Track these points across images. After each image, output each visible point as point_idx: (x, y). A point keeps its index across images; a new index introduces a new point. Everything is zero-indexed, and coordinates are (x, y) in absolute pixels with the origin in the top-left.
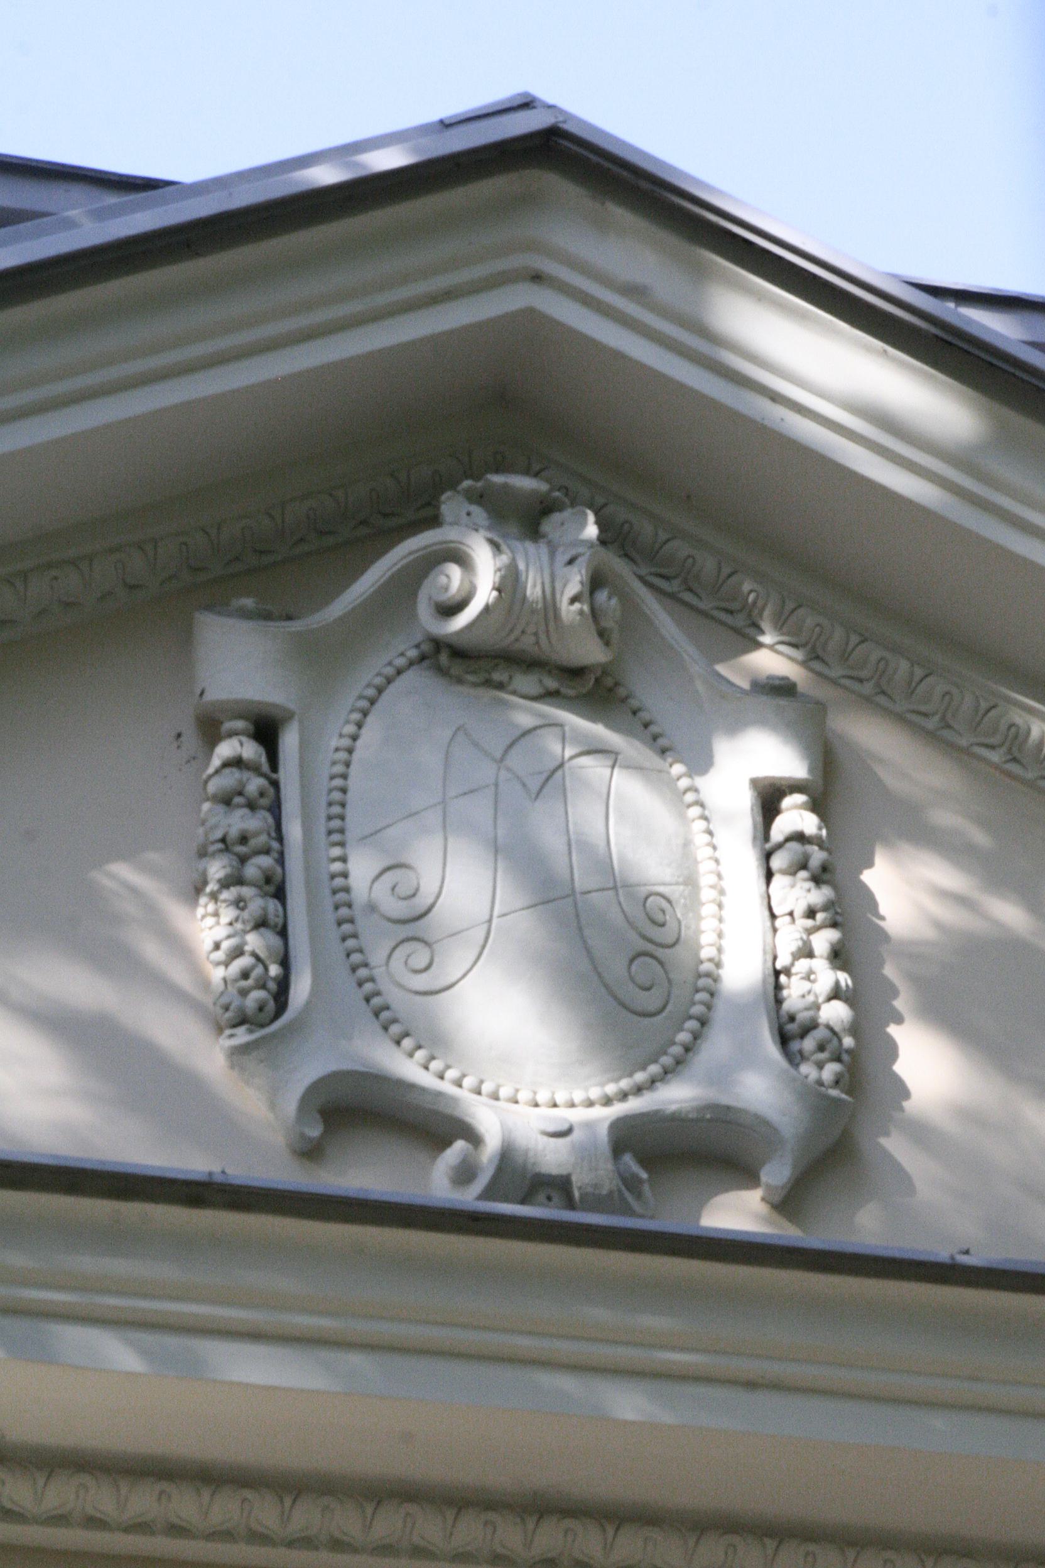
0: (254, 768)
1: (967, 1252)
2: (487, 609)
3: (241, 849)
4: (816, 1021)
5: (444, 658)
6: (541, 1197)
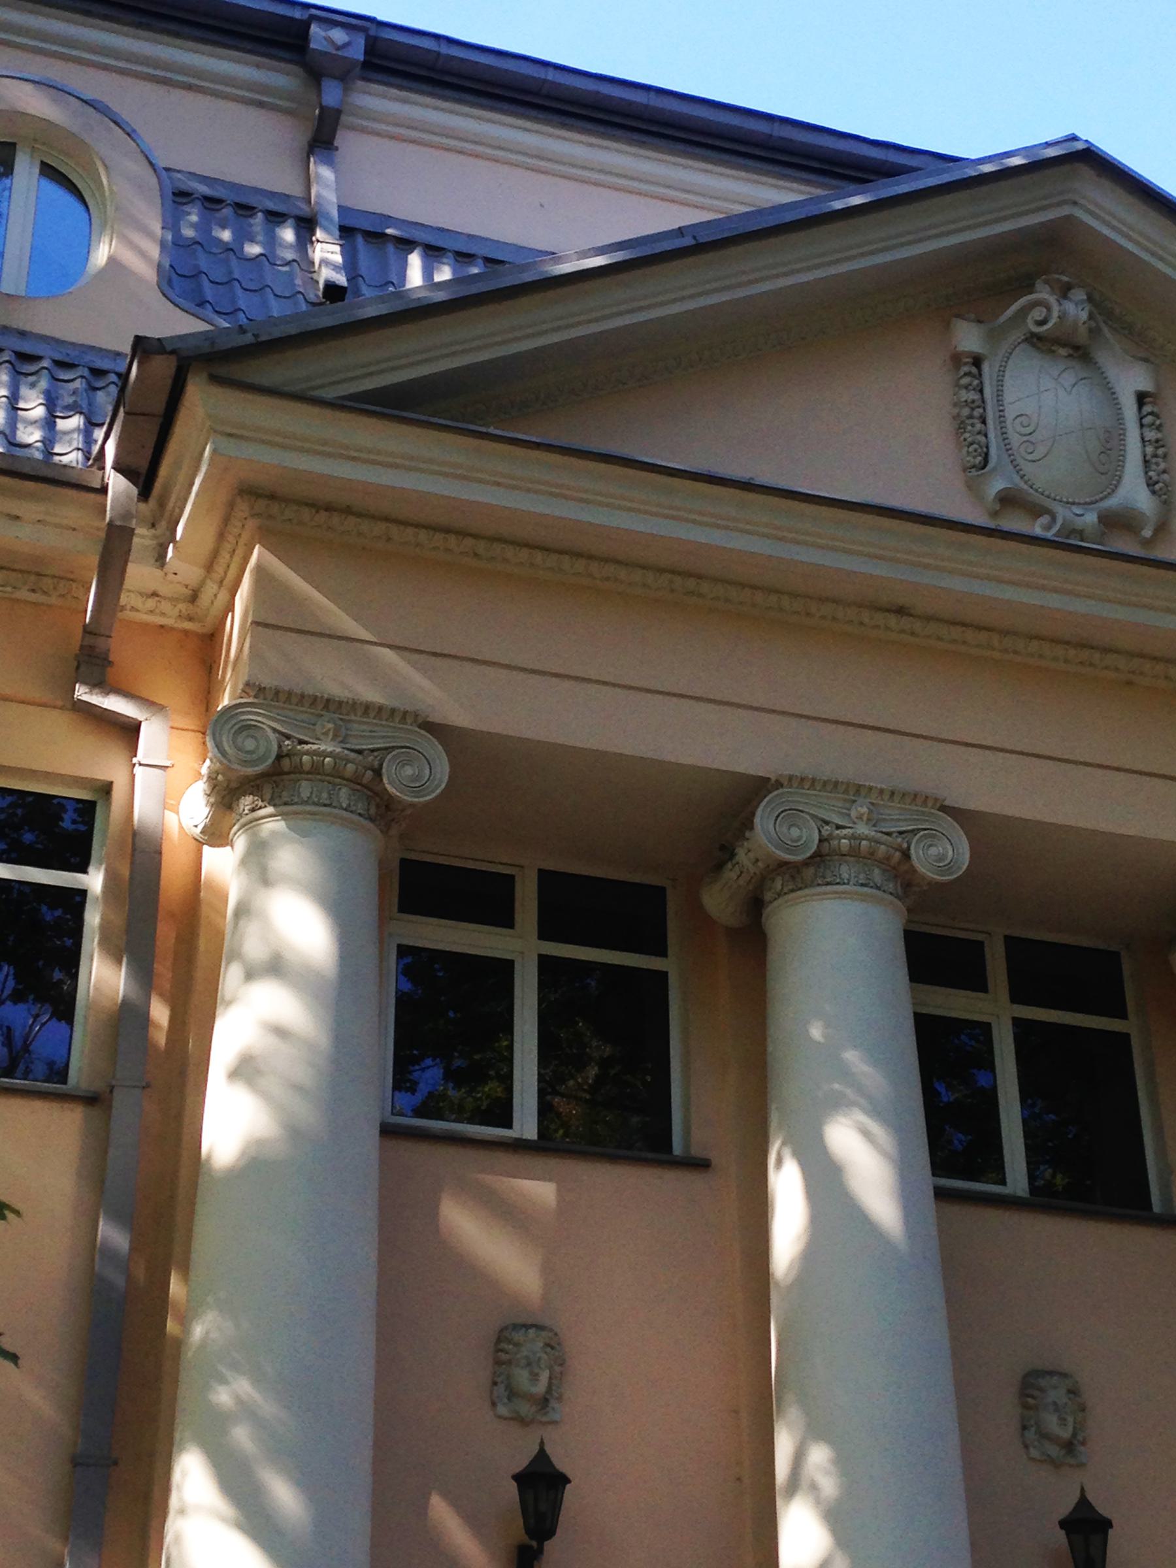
0: (974, 376)
1: (72, 572)
2: (1055, 324)
3: (973, 406)
4: (46, 418)
5: (1035, 340)
6: (1072, 536)
